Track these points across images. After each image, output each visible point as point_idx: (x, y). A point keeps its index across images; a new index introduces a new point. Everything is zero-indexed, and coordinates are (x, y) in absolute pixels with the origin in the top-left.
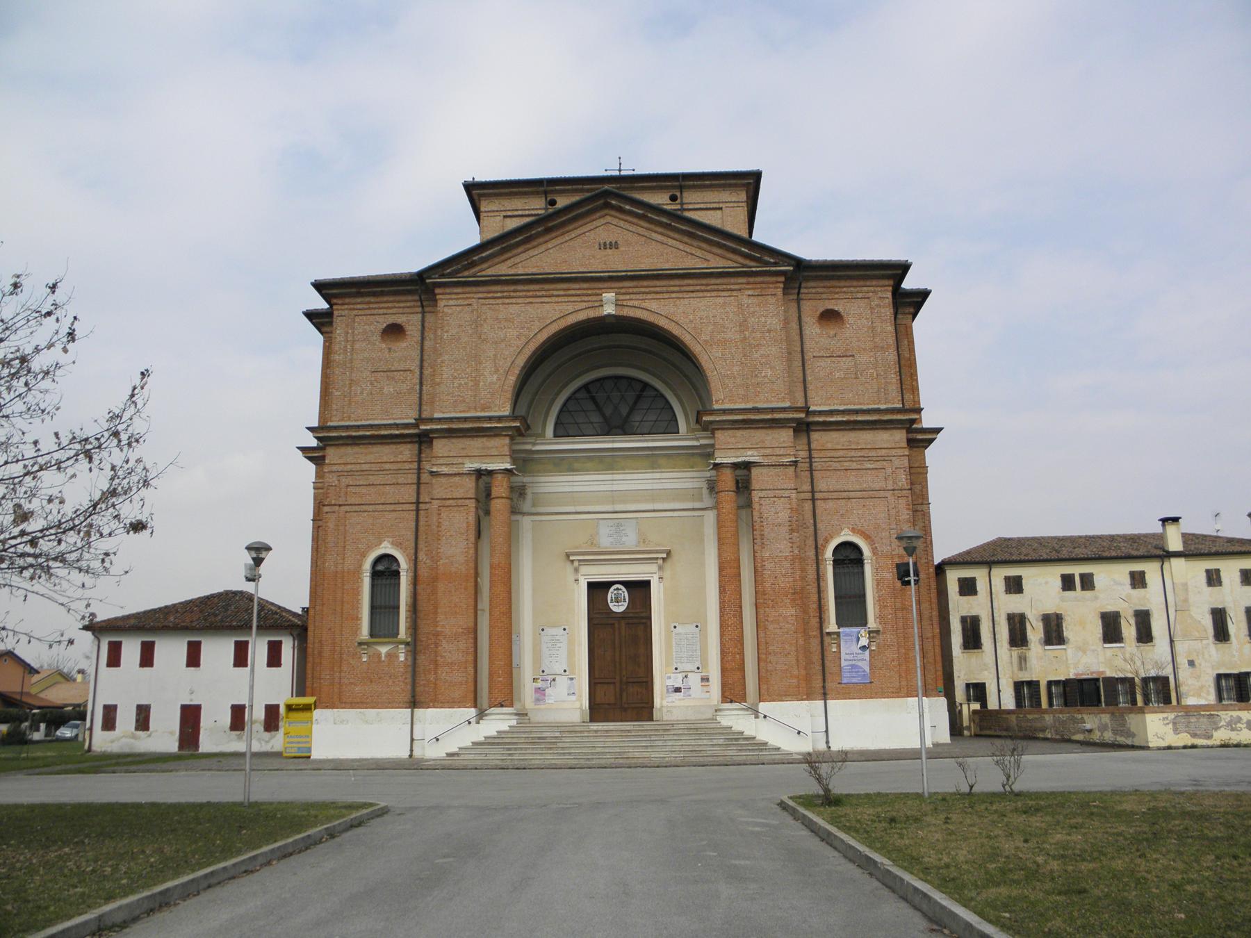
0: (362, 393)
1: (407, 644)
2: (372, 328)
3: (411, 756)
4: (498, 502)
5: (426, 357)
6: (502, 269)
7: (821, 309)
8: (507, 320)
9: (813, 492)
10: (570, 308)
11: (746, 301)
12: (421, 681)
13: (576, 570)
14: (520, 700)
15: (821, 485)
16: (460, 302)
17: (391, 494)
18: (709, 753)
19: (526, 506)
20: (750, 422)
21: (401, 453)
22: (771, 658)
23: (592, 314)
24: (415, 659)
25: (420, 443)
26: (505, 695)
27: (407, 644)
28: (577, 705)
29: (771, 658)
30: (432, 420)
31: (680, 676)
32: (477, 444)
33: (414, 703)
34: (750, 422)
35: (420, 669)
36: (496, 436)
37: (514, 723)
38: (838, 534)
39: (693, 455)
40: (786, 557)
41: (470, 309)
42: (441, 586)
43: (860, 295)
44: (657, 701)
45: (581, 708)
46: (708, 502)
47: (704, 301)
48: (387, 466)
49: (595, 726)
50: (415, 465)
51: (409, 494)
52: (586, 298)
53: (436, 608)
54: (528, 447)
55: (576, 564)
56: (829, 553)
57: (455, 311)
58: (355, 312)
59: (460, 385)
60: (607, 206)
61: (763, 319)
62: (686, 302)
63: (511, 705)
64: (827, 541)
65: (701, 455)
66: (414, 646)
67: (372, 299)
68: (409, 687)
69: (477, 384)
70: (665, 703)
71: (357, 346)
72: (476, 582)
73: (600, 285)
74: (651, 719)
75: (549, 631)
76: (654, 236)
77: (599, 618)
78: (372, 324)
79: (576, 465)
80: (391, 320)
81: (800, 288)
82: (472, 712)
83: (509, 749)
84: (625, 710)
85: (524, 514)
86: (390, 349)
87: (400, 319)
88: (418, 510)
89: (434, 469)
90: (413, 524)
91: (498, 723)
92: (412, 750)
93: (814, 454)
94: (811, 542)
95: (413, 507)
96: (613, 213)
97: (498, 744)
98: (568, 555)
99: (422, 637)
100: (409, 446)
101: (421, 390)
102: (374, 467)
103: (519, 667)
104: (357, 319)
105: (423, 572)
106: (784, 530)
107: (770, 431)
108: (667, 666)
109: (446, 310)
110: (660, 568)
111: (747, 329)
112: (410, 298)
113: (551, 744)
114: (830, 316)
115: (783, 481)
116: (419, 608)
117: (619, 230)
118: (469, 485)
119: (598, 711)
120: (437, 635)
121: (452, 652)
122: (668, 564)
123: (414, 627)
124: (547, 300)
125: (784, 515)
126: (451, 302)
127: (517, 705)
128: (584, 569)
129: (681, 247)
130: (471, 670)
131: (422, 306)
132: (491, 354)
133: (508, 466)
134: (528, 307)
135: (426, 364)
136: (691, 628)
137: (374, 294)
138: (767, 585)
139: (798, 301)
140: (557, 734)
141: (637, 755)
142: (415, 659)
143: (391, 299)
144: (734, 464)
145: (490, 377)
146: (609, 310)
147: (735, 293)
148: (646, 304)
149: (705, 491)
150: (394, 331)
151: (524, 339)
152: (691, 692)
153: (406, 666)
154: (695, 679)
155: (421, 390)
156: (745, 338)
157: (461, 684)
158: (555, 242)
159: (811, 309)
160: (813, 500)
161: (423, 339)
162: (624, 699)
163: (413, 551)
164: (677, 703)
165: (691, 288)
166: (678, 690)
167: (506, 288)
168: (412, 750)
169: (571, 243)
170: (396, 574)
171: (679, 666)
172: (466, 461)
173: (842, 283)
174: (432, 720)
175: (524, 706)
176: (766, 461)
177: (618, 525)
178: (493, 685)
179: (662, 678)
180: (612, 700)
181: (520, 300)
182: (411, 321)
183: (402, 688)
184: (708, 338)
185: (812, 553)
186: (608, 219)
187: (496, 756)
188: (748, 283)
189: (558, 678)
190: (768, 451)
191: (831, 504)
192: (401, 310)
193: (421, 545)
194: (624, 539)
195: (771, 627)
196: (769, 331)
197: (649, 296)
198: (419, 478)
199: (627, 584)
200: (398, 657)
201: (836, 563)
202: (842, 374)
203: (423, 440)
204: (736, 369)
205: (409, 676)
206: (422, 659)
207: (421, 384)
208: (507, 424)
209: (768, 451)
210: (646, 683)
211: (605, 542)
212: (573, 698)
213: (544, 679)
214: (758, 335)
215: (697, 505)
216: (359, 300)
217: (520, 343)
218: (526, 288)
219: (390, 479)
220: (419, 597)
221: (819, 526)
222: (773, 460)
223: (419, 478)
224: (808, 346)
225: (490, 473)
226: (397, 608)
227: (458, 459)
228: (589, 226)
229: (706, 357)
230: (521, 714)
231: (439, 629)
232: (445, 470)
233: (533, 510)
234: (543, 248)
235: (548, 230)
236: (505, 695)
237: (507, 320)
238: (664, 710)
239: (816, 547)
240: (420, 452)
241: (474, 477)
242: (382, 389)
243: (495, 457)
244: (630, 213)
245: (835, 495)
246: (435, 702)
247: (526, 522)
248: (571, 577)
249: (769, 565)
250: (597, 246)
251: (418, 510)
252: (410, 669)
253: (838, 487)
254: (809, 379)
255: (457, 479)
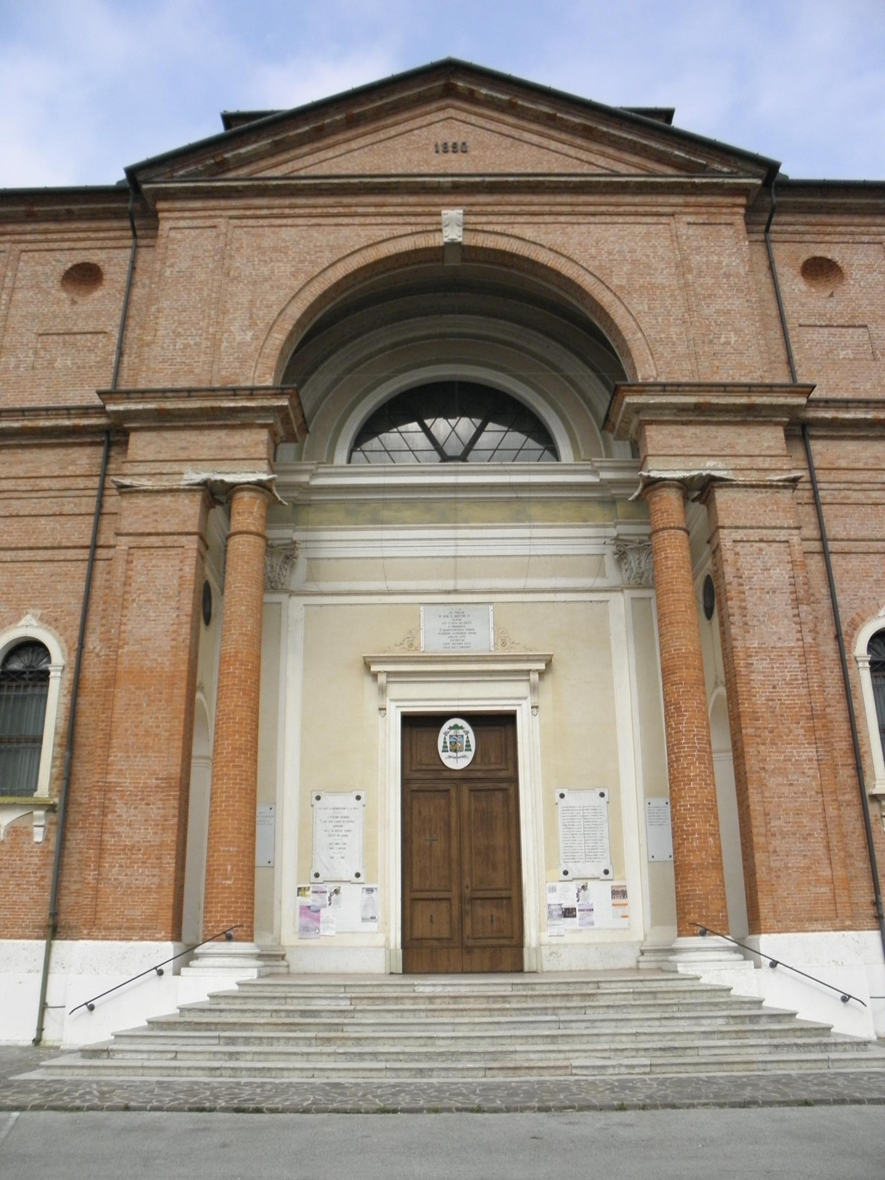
0: (17, 367)
1: (51, 808)
2: (47, 270)
3: (37, 1041)
4: (246, 554)
5: (133, 312)
6: (276, 170)
7: (805, 257)
8: (275, 249)
9: (823, 539)
10: (385, 232)
11: (683, 230)
12: (72, 882)
13: (382, 691)
14: (271, 929)
15: (834, 529)
16: (196, 223)
17: (48, 531)
18: (705, 1056)
19: (297, 577)
20: (714, 406)
21: (73, 462)
22: (777, 843)
23: (422, 242)
24: (62, 840)
25: (109, 445)
26: (241, 919)
27: (51, 808)
28: (380, 940)
29: (777, 843)
30: (128, 395)
31: (573, 887)
32: (208, 441)
33: (54, 929)
34: (714, 406)
35: (72, 860)
36: (244, 426)
37: (251, 974)
38: (873, 614)
39: (587, 500)
40: (790, 650)
41: (213, 233)
42: (122, 696)
43: (866, 239)
44: (532, 935)
45: (386, 947)
46: (613, 576)
47: (613, 230)
48: (45, 484)
49: (429, 985)
50: (95, 482)
51: (80, 531)
52: (412, 219)
53: (109, 736)
54: (304, 478)
55: (382, 679)
56: (860, 647)
57: (187, 237)
58: (23, 246)
59: (186, 346)
60: (450, 92)
61: (715, 258)
62: (583, 228)
63: (250, 938)
64: (855, 626)
65: (602, 502)
66: (63, 813)
67: (52, 226)
68: (48, 896)
69: (216, 344)
70: (545, 938)
71: (18, 296)
72: (64, 334)
73: (437, 199)
74: (519, 969)
75: (329, 800)
76: (527, 136)
77: (421, 779)
78: (48, 262)
79: (386, 514)
80: (80, 257)
81: (767, 231)
82: (167, 949)
83: (232, 1041)
84: (469, 950)
85: (291, 593)
86: (74, 302)
87: (95, 257)
88: (93, 560)
89: (127, 481)
90: (82, 585)
91: (221, 972)
92: (40, 1029)
93: (820, 476)
94: (826, 628)
95: (85, 554)
96: (458, 104)
97: (208, 1026)
98: (367, 665)
99: (79, 797)
100: (88, 450)
101: (119, 362)
102: (23, 485)
103: (271, 865)
104: (24, 257)
105: (93, 671)
106: (782, 602)
107: (743, 430)
108: (549, 866)
109: (173, 234)
110: (534, 689)
111: (690, 270)
112: (115, 224)
113: (330, 1030)
114: (819, 270)
115: (780, 511)
116: (80, 740)
117: (469, 128)
118: (190, 509)
119: (420, 952)
120: (106, 789)
121: (135, 823)
122: (548, 679)
123: (67, 777)
124: (345, 220)
125: (780, 574)
126: (182, 223)
127: (263, 940)
128: (396, 690)
129: (572, 152)
130: (170, 863)
131: (135, 236)
132: (245, 299)
133: (264, 477)
134: (314, 232)
135: (132, 323)
136: (591, 799)
137: (56, 218)
138: (760, 700)
139: (767, 242)
140: (345, 1005)
141: (536, 1060)
142: (62, 840)
143: (84, 225)
144: (682, 481)
145: (240, 334)
146: (453, 234)
147: (664, 220)
148: (516, 230)
149: (609, 562)
150: (84, 276)
151: (303, 278)
152: (594, 916)
153: (45, 853)
154: (599, 893)
155: (119, 362)
156: (687, 285)
157: (149, 890)
158: (362, 141)
159: (789, 257)
160: (825, 553)
161: (131, 284)
162: (468, 931)
163: (77, 633)
164: (569, 938)
165: (592, 209)
166: (569, 913)
167: (277, 202)
168: (40, 1029)
169: (389, 144)
170: (44, 677)
171: (570, 867)
172: (187, 468)
173: (836, 219)
174: (84, 963)
175: (278, 939)
176: (740, 478)
177: (458, 615)
178: (209, 894)
179: (541, 889)
180: (445, 932)
181: (300, 221)
182: (113, 261)
183: (34, 900)
184: (624, 282)
185: (829, 648)
186: (451, 112)
187: (197, 1063)
188: (687, 205)
189: (344, 888)
190: (744, 462)
191: (854, 562)
192: (99, 244)
193: (94, 622)
194: (469, 638)
195: (772, 782)
196: (727, 276)
197: (520, 219)
198: (100, 505)
199: (476, 719)
200: (30, 834)
201: (876, 667)
202: (850, 353)
203: (113, 436)
204: (674, 331)
205: (49, 873)
206: (76, 839)
207: (121, 354)
208: (266, 403)
209: (744, 462)
210: (511, 900)
211: (432, 637)
212: (372, 926)
213: (319, 890)
214: (709, 281)
215: (599, 583)
216: (29, 227)
217: (297, 284)
218: (311, 201)
219: (49, 506)
220: (82, 720)
221: (840, 598)
222: (753, 477)
223: (100, 505)
224: (789, 308)
225: (233, 488)
226: (38, 740)
227: (172, 464)
228: (419, 122)
229: (621, 310)
230: (271, 957)
231: (112, 778)
232: (146, 483)
233: (312, 587)
234: (344, 148)
235: (352, 122)
236: (241, 919)
237: (275, 249)
238: (545, 951)
239: (838, 637)
240: (107, 459)
241: (198, 497)
242: (51, 362)
243: (241, 458)
244: (490, 103)
245: (862, 546)
246: (95, 927)
247: (295, 607)
248: (371, 701)
249: (759, 664)
250: (432, 148)
251: (93, 560)
252: (52, 859)
253: (863, 534)
254: (796, 357)
255: (167, 500)
